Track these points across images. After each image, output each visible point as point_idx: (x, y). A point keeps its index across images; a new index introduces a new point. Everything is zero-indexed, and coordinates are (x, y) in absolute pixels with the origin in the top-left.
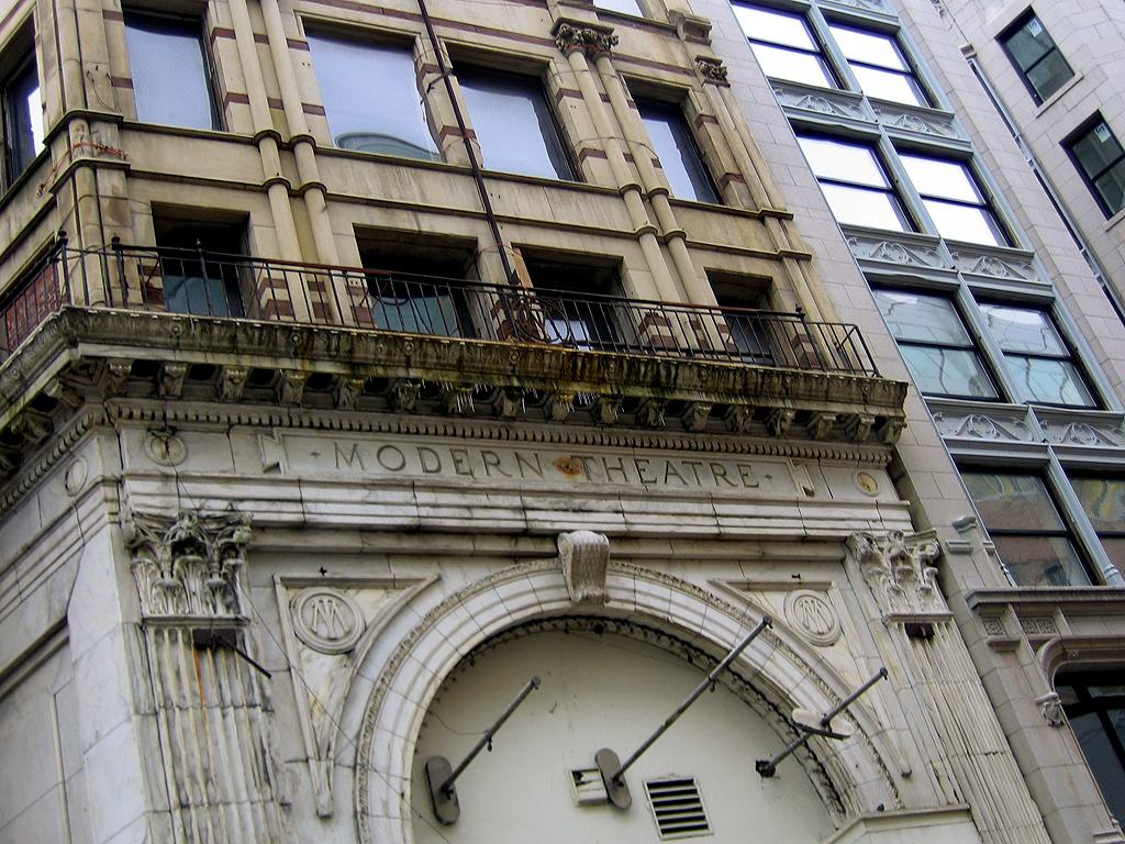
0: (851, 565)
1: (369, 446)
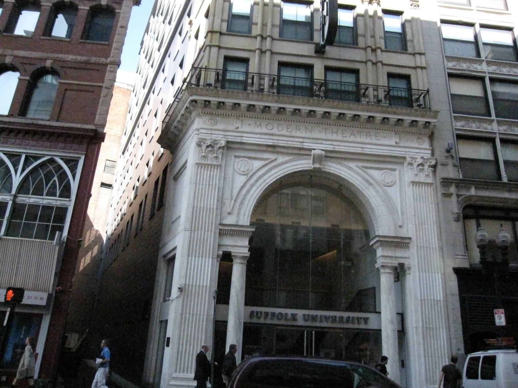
0: (406, 164)
1: (264, 123)
